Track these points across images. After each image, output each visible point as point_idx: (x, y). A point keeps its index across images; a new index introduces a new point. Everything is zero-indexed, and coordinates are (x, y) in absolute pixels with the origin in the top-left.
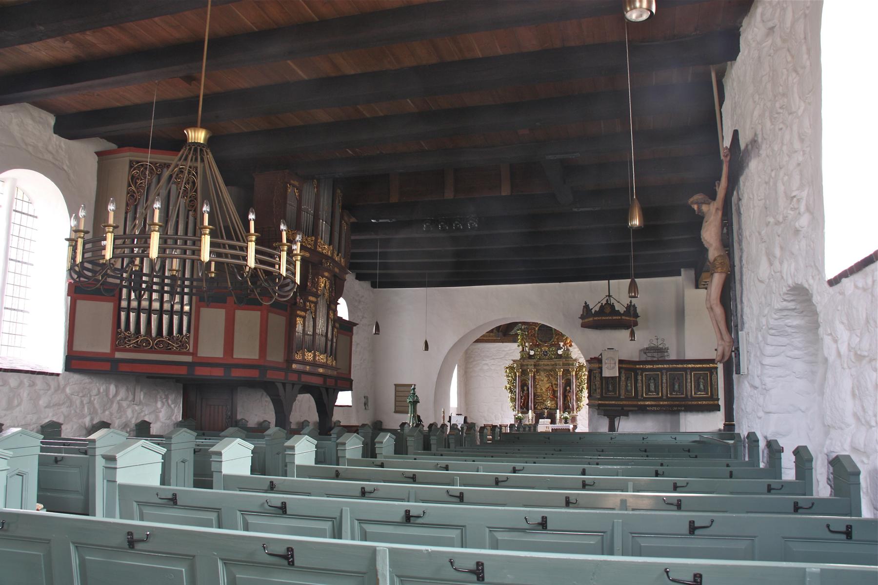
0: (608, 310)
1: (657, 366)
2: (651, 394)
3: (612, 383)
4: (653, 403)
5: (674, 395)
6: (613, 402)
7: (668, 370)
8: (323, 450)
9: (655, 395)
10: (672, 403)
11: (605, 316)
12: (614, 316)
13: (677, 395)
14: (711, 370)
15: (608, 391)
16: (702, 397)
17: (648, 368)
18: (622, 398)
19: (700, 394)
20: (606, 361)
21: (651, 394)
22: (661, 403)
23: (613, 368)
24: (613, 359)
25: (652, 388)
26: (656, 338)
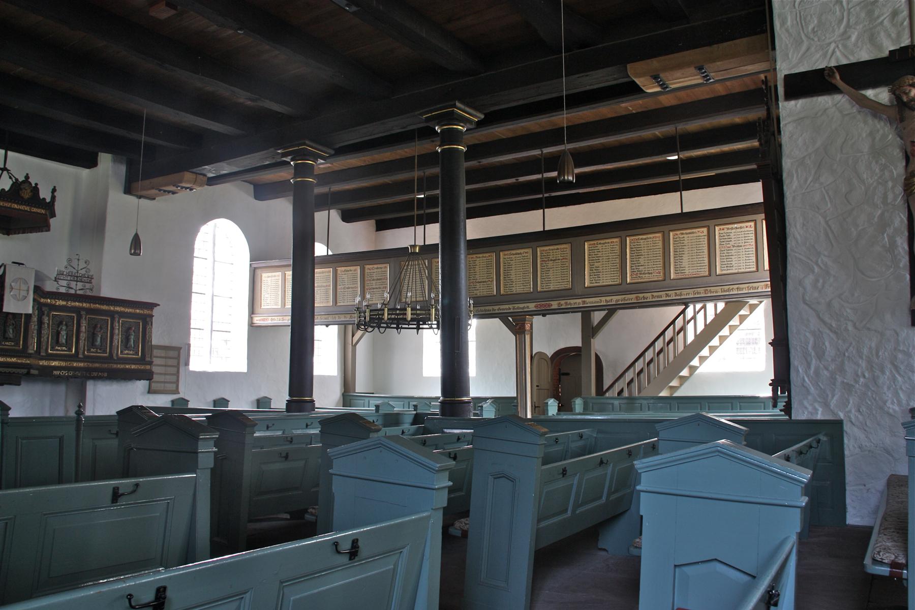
0: (26, 194)
1: (73, 304)
2: (59, 348)
3: (13, 324)
4: (63, 364)
5: (93, 352)
6: (14, 360)
7: (89, 311)
8: (363, 401)
9: (64, 351)
10: (90, 365)
11: (17, 203)
12: (35, 207)
13: (97, 352)
14: (80, 312)
15: (6, 339)
16: (129, 358)
17: (59, 306)
18: (31, 354)
19: (128, 354)
20: (12, 284)
21: (59, 348)
22: (75, 364)
23: (25, 298)
24: (26, 282)
25: (63, 340)
26: (77, 257)
